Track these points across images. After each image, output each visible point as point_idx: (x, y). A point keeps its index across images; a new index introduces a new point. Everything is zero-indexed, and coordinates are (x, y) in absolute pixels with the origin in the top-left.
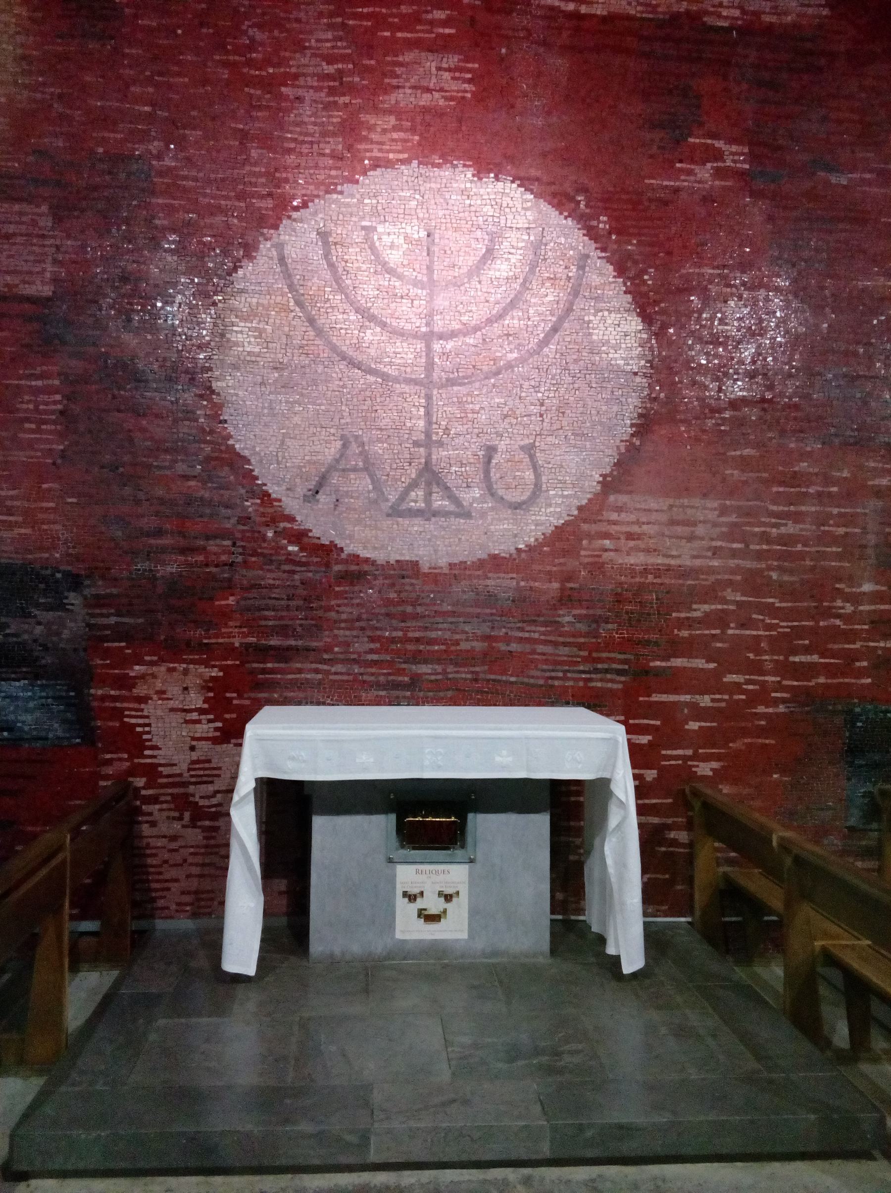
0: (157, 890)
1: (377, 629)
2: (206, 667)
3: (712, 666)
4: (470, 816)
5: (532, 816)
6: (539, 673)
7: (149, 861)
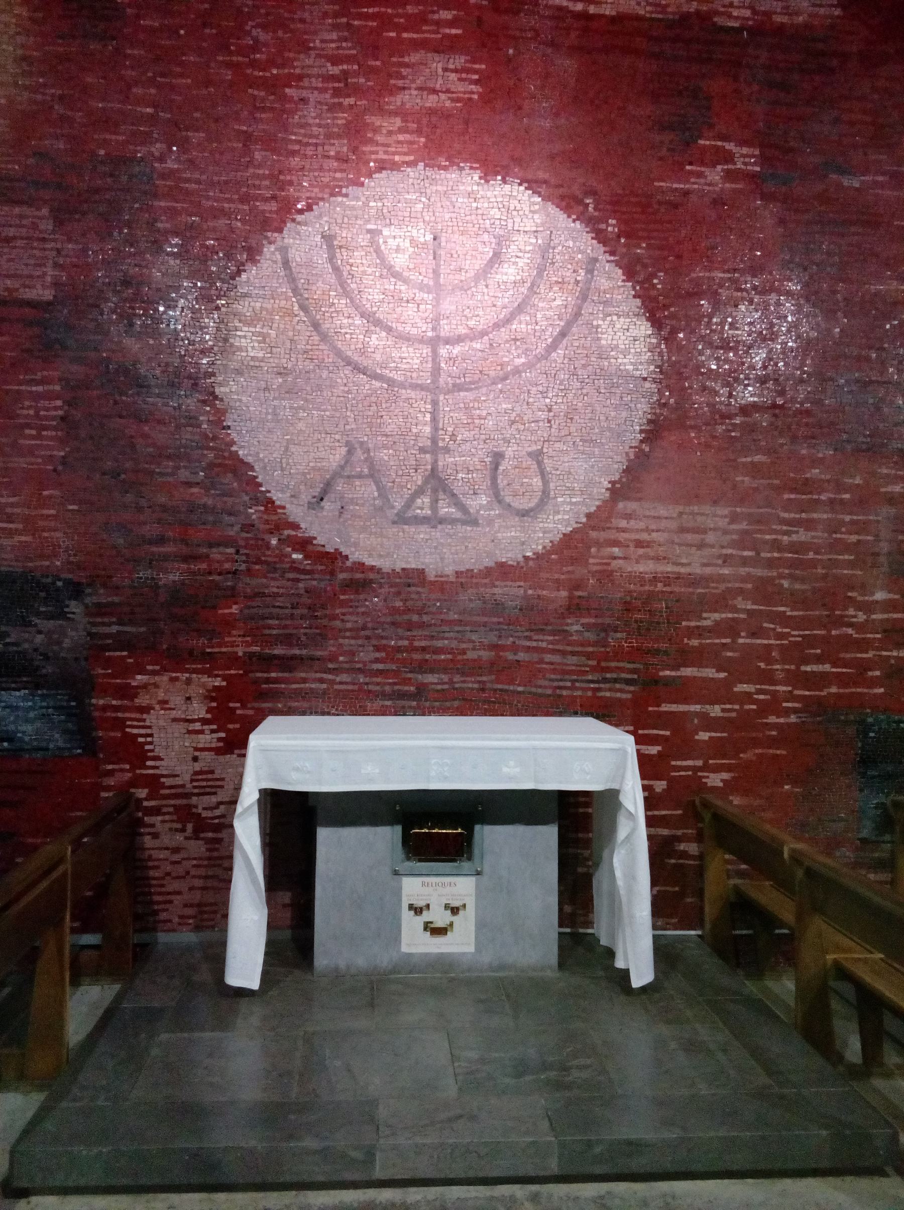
0: (159, 903)
1: (382, 638)
2: (209, 677)
3: (722, 675)
4: (477, 828)
5: (540, 828)
6: (546, 683)
7: (152, 873)
